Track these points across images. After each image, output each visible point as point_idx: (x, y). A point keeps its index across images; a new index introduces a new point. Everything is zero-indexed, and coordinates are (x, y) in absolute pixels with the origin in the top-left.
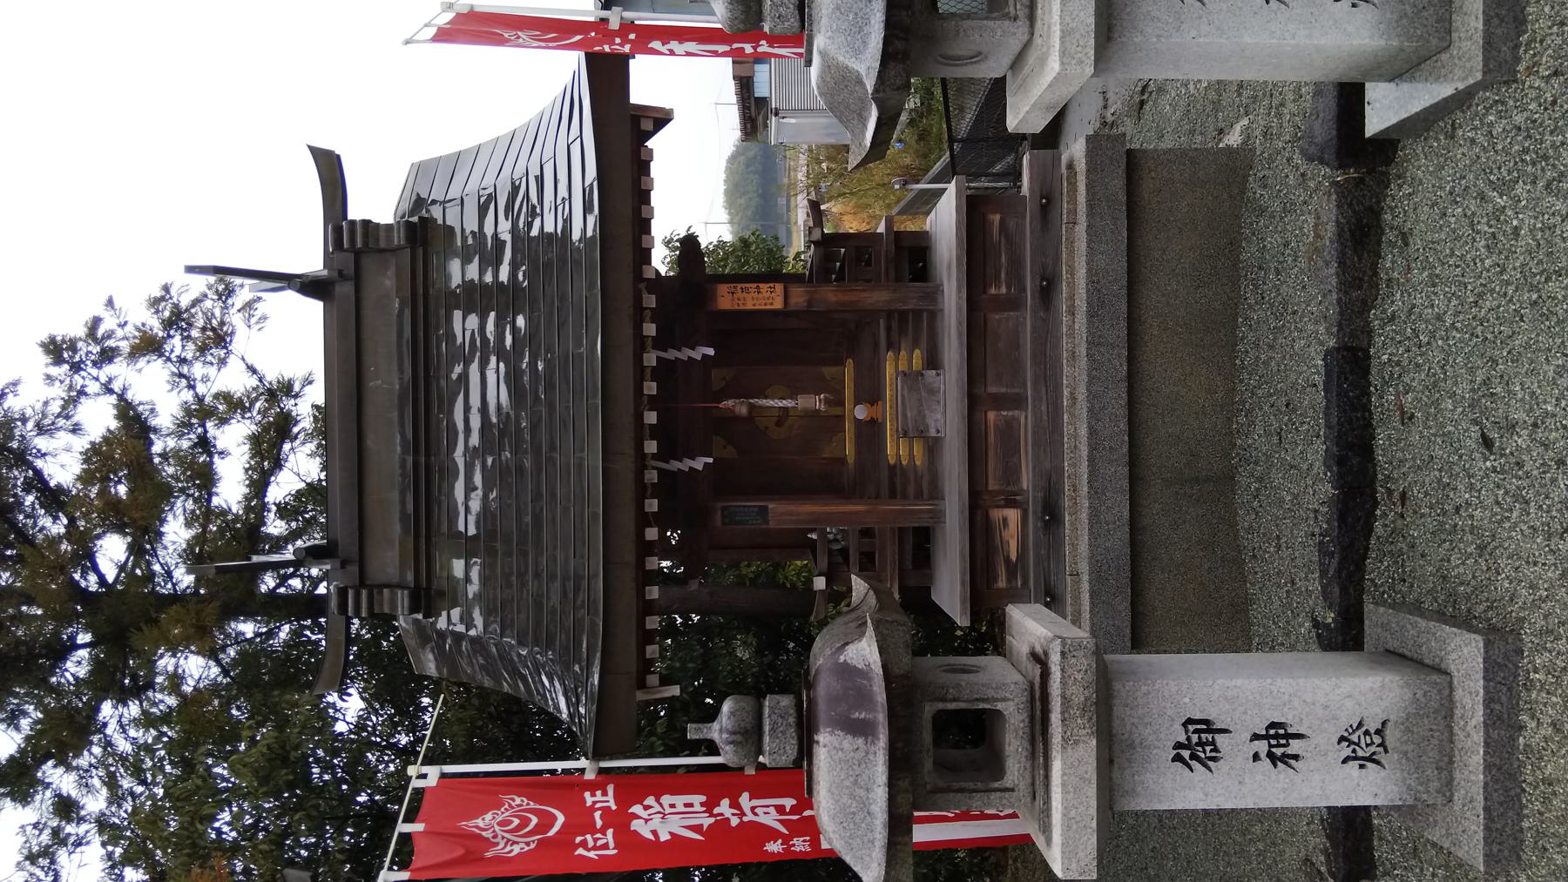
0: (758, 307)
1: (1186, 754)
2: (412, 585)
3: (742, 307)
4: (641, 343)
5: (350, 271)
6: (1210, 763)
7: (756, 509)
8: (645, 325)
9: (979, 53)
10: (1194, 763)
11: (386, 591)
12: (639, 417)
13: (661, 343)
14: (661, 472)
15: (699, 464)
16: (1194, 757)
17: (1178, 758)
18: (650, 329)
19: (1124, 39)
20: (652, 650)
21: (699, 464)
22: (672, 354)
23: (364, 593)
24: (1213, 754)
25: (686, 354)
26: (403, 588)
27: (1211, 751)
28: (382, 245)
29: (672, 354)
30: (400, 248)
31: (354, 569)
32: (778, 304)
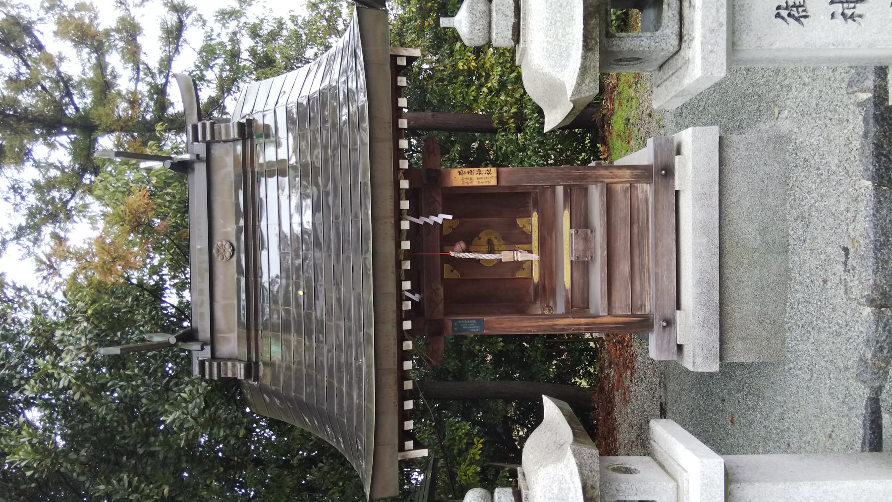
0: (481, 184)
1: (784, 13)
2: (246, 360)
3: (470, 185)
4: (399, 215)
5: (203, 155)
6: (802, 20)
7: (474, 321)
8: (402, 202)
9: (639, 59)
10: (790, 20)
11: (229, 364)
12: (397, 184)
13: (415, 211)
14: (411, 223)
15: (440, 218)
16: (789, 15)
17: (778, 15)
18: (405, 205)
19: (744, 12)
20: (408, 365)
21: (440, 218)
22: (421, 221)
23: (215, 364)
24: (804, 14)
25: (432, 220)
26: (240, 361)
27: (803, 11)
28: (224, 138)
29: (421, 221)
30: (234, 140)
31: (208, 349)
32: (493, 182)
